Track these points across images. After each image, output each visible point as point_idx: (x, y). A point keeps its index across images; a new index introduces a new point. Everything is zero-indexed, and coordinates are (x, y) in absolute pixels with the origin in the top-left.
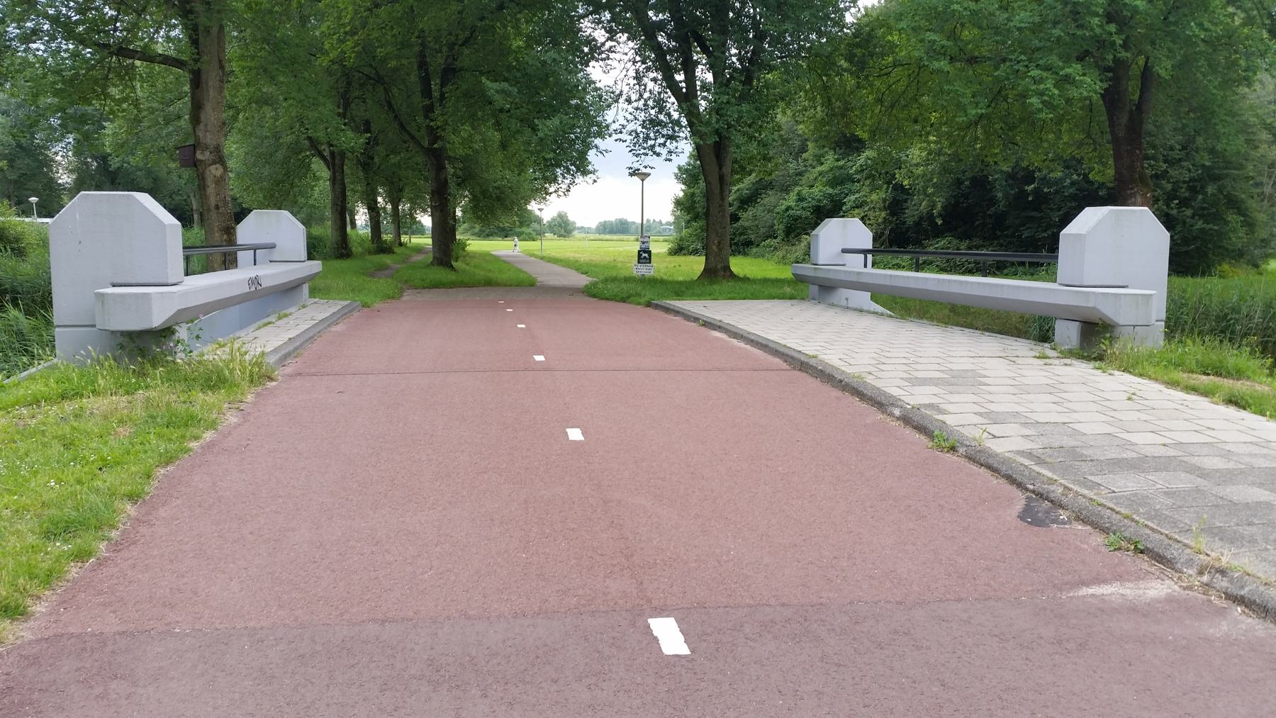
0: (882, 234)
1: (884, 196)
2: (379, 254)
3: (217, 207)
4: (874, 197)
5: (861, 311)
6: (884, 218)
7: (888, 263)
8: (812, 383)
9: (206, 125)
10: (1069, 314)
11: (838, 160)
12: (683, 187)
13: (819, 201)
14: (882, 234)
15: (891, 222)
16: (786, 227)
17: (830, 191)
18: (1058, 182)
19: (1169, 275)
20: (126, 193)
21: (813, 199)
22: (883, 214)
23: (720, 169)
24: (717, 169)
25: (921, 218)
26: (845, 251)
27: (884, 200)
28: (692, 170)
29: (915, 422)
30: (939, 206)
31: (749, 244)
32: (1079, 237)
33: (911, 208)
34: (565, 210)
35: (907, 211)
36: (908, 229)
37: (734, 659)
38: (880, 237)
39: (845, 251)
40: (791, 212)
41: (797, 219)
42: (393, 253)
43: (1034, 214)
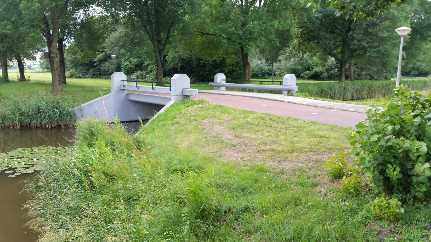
3: (57, 69)
8: (266, 100)
9: (53, 47)
10: (285, 90)
13: (136, 63)
17: (139, 60)
18: (209, 61)
19: (190, 83)
20: (328, 82)
25: (170, 69)
26: (222, 80)
29: (289, 102)
30: (179, 66)
31: (100, 74)
32: (287, 79)
37: (206, 160)
39: (222, 80)
43: (202, 68)
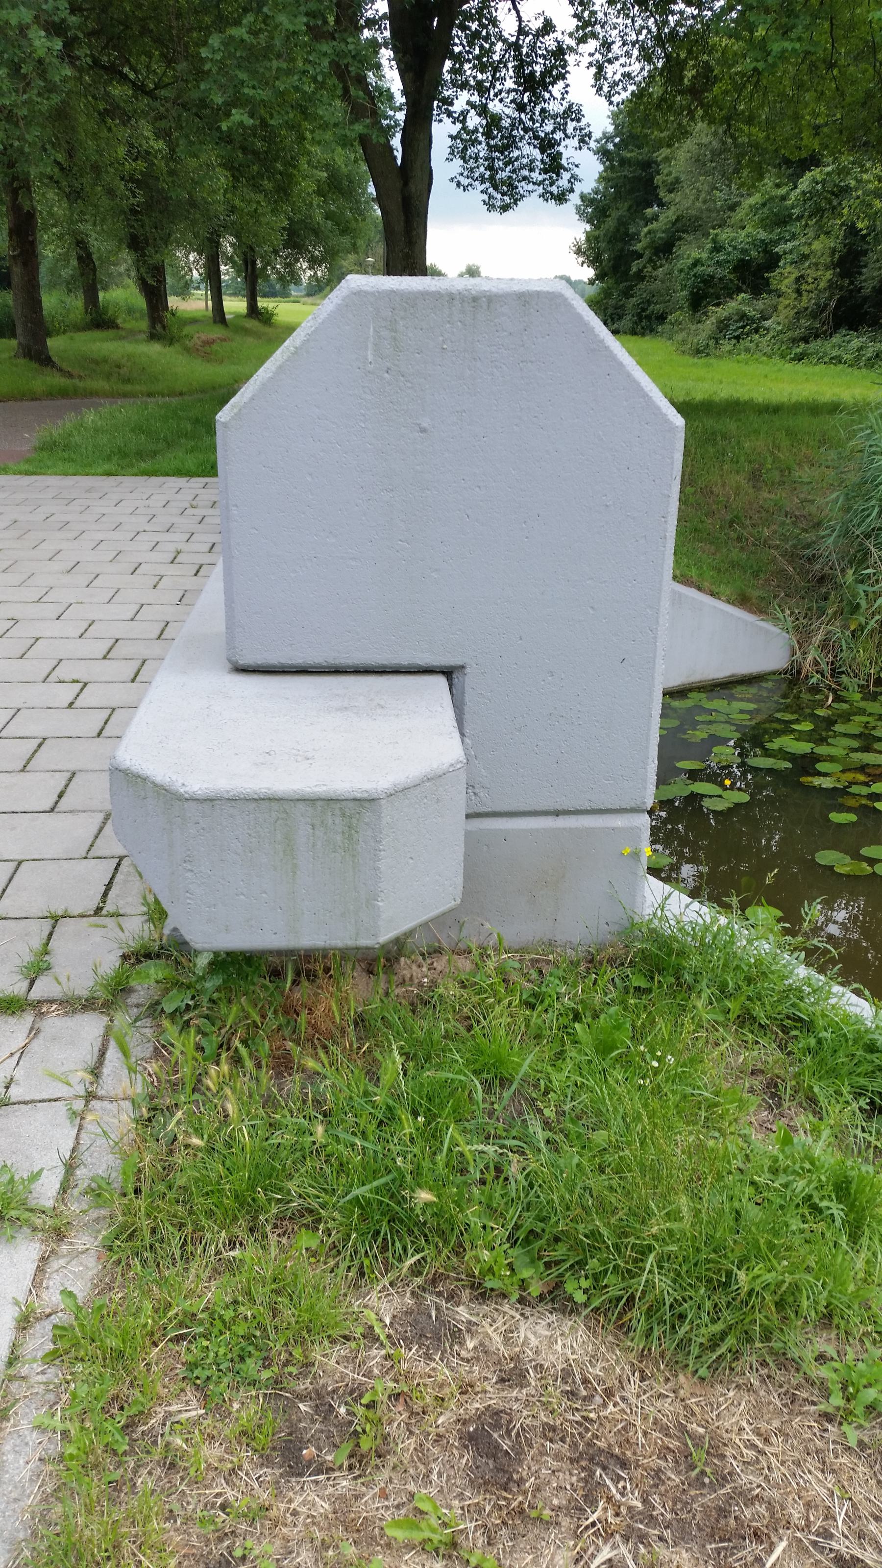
0: (826, 306)
1: (832, 245)
2: (89, 329)
4: (817, 246)
5: (96, 837)
6: (830, 281)
7: (825, 354)
11: (778, 186)
12: (588, 227)
13: (744, 251)
14: (826, 306)
15: (841, 288)
16: (692, 293)
21: (735, 248)
22: (829, 275)
23: (406, 184)
24: (399, 184)
27: (833, 251)
28: (601, 201)
33: (871, 266)
34: (477, 263)
35: (864, 270)
36: (865, 299)
38: (822, 312)
40: (700, 269)
41: (708, 280)
42: (116, 327)
